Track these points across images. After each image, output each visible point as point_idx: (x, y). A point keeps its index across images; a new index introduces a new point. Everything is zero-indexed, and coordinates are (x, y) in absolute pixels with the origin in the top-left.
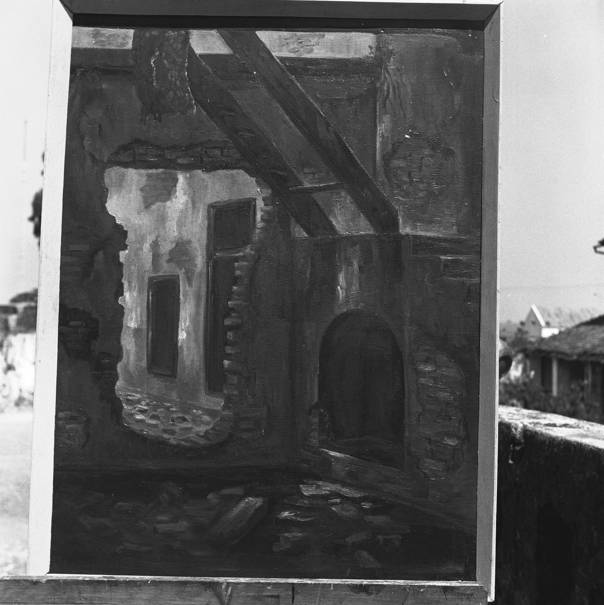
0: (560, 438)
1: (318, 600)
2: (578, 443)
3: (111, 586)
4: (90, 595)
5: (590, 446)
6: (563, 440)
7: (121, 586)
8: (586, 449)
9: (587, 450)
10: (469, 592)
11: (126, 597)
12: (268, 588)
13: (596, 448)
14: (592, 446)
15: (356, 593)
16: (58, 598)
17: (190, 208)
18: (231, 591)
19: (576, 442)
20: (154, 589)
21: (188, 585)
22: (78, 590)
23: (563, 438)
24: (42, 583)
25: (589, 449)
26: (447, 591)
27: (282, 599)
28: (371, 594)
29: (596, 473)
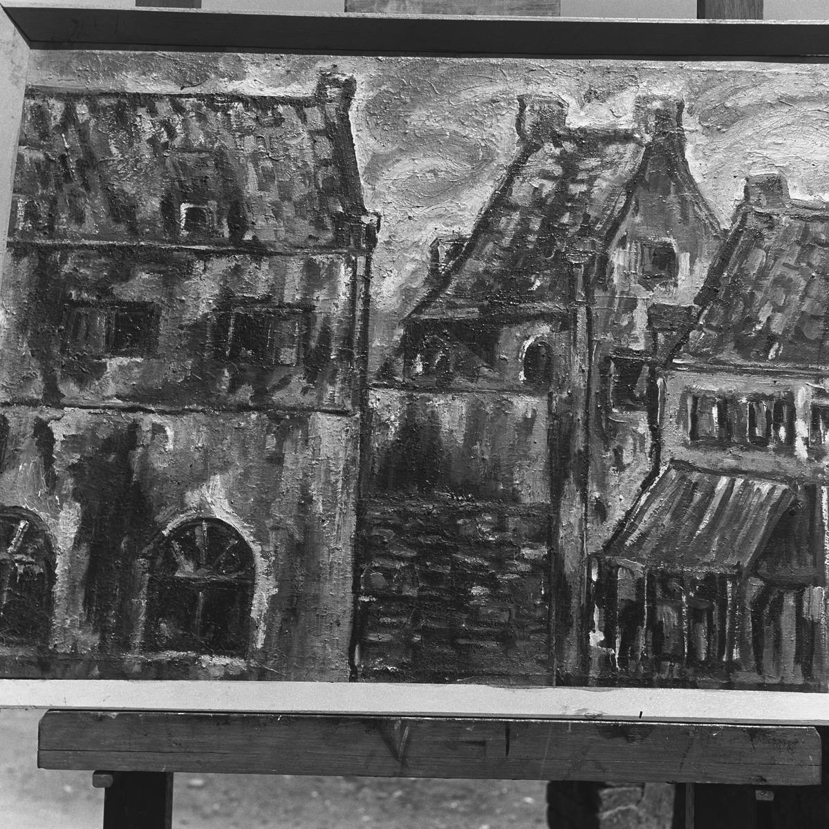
3: (218, 724)
4: (185, 739)
10: (790, 738)
18: (409, 735)
21: (340, 724)
24: (111, 718)
28: (633, 740)
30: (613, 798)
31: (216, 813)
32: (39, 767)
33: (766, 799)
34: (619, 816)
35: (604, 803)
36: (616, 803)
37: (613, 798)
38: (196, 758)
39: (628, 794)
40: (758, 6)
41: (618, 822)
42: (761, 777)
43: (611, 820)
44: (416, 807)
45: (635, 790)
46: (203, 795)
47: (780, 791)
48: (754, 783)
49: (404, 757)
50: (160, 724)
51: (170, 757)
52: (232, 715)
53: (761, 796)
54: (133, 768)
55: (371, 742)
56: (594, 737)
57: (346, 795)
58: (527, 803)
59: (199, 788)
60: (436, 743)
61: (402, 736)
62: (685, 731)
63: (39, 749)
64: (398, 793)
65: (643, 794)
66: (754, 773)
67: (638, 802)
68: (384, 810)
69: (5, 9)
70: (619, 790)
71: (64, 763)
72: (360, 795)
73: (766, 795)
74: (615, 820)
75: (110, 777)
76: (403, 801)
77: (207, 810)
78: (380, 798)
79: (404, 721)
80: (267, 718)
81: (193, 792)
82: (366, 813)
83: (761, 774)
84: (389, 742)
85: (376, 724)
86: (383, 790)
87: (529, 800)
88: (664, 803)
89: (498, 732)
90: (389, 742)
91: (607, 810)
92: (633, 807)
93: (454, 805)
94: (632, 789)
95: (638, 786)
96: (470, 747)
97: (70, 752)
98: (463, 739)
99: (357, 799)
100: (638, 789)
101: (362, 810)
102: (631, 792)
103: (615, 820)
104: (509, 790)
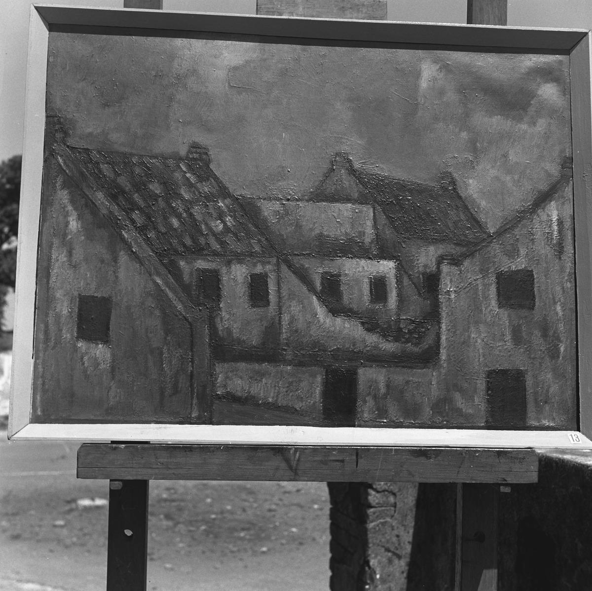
0: (540, 455)
1: (380, 464)
2: (560, 459)
3: (186, 451)
4: (165, 460)
5: (573, 462)
6: (544, 456)
7: (195, 452)
8: (568, 464)
9: (570, 465)
10: (520, 456)
11: (201, 462)
12: (334, 453)
13: (579, 464)
14: (575, 462)
15: (416, 457)
16: (136, 463)
17: (88, 348)
18: (299, 456)
19: (557, 458)
20: (226, 455)
21: (258, 451)
22: (155, 455)
23: (544, 455)
24: (121, 448)
25: (571, 465)
26: (501, 455)
27: (346, 463)
28: (430, 458)
29: (579, 488)
30: (376, 514)
31: (74, 544)
32: (78, 478)
33: (506, 491)
34: (380, 525)
35: (371, 517)
36: (378, 517)
37: (376, 514)
38: (173, 471)
39: (386, 512)
40: (504, 20)
41: (379, 529)
42: (504, 478)
43: (375, 529)
44: (216, 536)
45: (390, 509)
46: (65, 532)
47: (515, 487)
48: (500, 482)
49: (296, 470)
50: (151, 452)
51: (157, 471)
52: (193, 446)
53: (503, 489)
54: (135, 478)
55: (277, 461)
56: (408, 457)
57: (167, 530)
58: (293, 532)
59: (62, 527)
60: (314, 461)
61: (295, 457)
62: (460, 453)
63: (78, 467)
64: (203, 528)
65: (395, 511)
66: (500, 477)
67: (392, 516)
68: (194, 539)
69: (37, 8)
70: (380, 509)
71: (92, 475)
72: (177, 530)
73: (507, 489)
74: (377, 528)
75: (121, 483)
76: (207, 533)
77: (68, 542)
78: (190, 531)
79: (295, 448)
80: (215, 447)
81: (57, 530)
82: (181, 541)
83: (504, 477)
84: (287, 461)
85: (279, 450)
86: (192, 526)
87: (294, 530)
88: (409, 517)
89: (351, 454)
90: (287, 461)
91: (372, 522)
92: (388, 519)
93: (242, 534)
94: (388, 508)
95: (393, 506)
96: (335, 463)
97: (96, 469)
98: (331, 458)
99: (174, 532)
100: (393, 508)
101: (178, 539)
102: (387, 510)
103: (377, 528)
104: (280, 523)
